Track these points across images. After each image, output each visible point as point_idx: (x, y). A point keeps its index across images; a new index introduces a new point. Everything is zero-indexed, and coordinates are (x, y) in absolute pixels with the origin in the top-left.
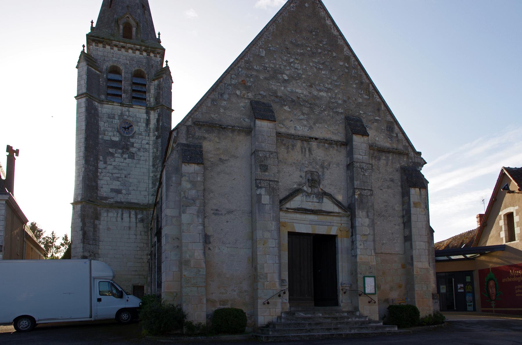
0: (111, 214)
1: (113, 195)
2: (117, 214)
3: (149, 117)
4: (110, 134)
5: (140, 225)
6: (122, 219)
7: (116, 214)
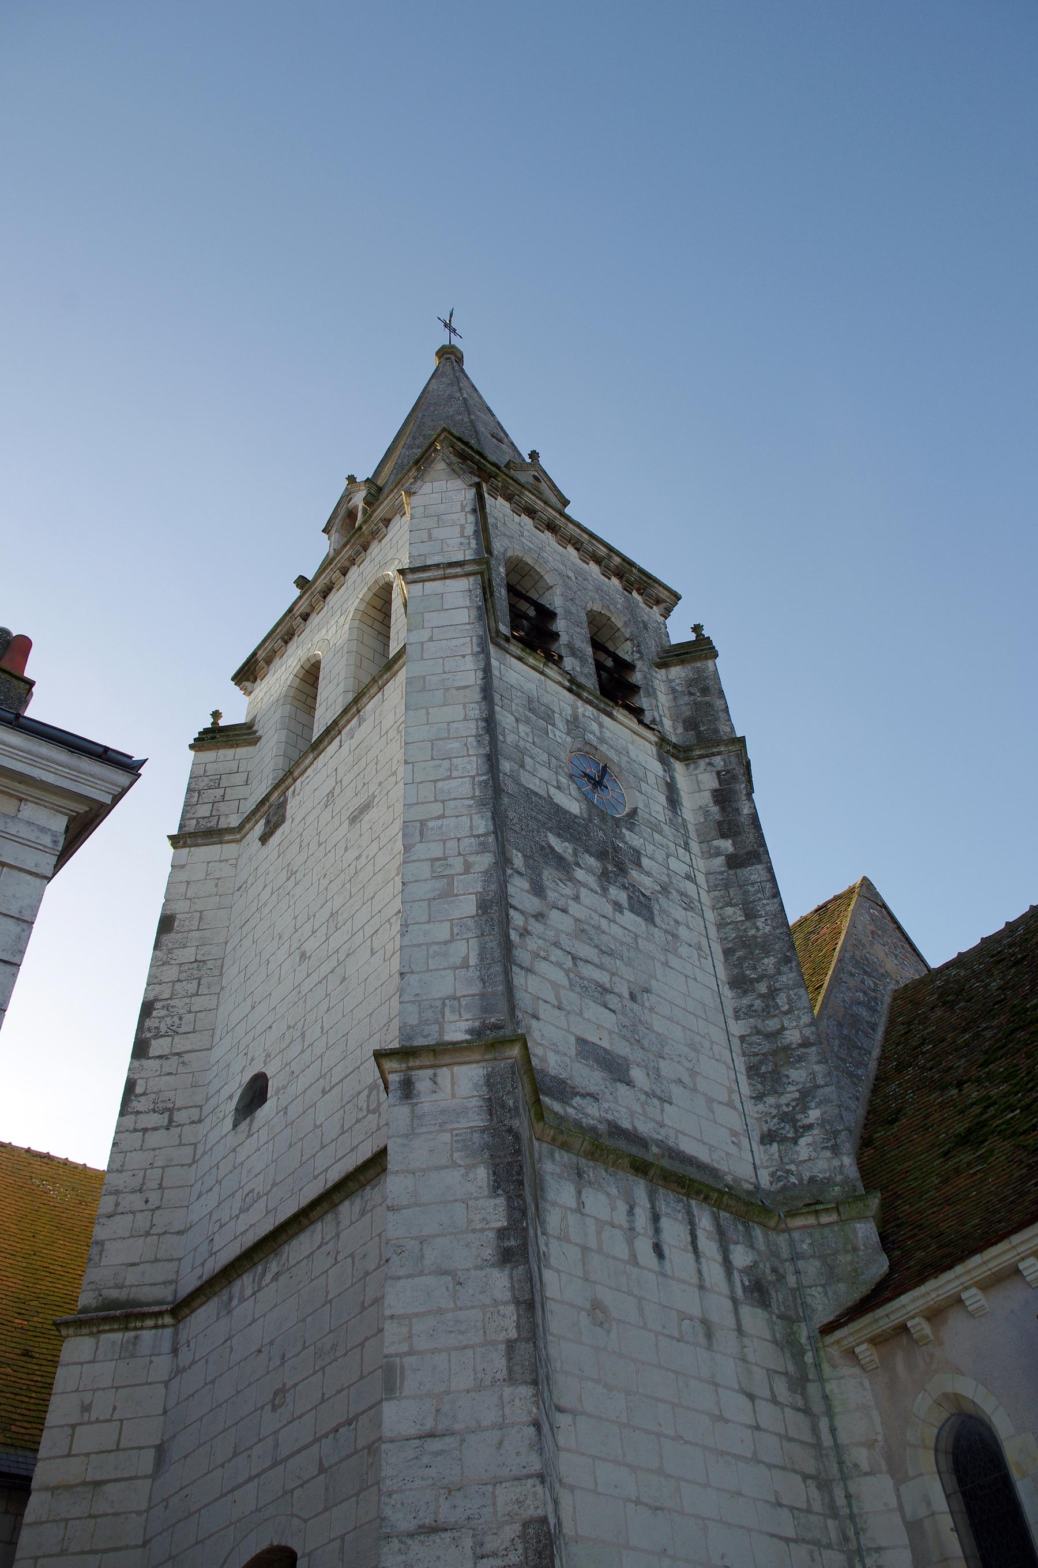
0: (596, 1203)
1: (587, 1077)
2: (631, 1212)
3: (672, 778)
4: (544, 773)
5: (754, 1318)
6: (658, 1249)
7: (622, 1207)
